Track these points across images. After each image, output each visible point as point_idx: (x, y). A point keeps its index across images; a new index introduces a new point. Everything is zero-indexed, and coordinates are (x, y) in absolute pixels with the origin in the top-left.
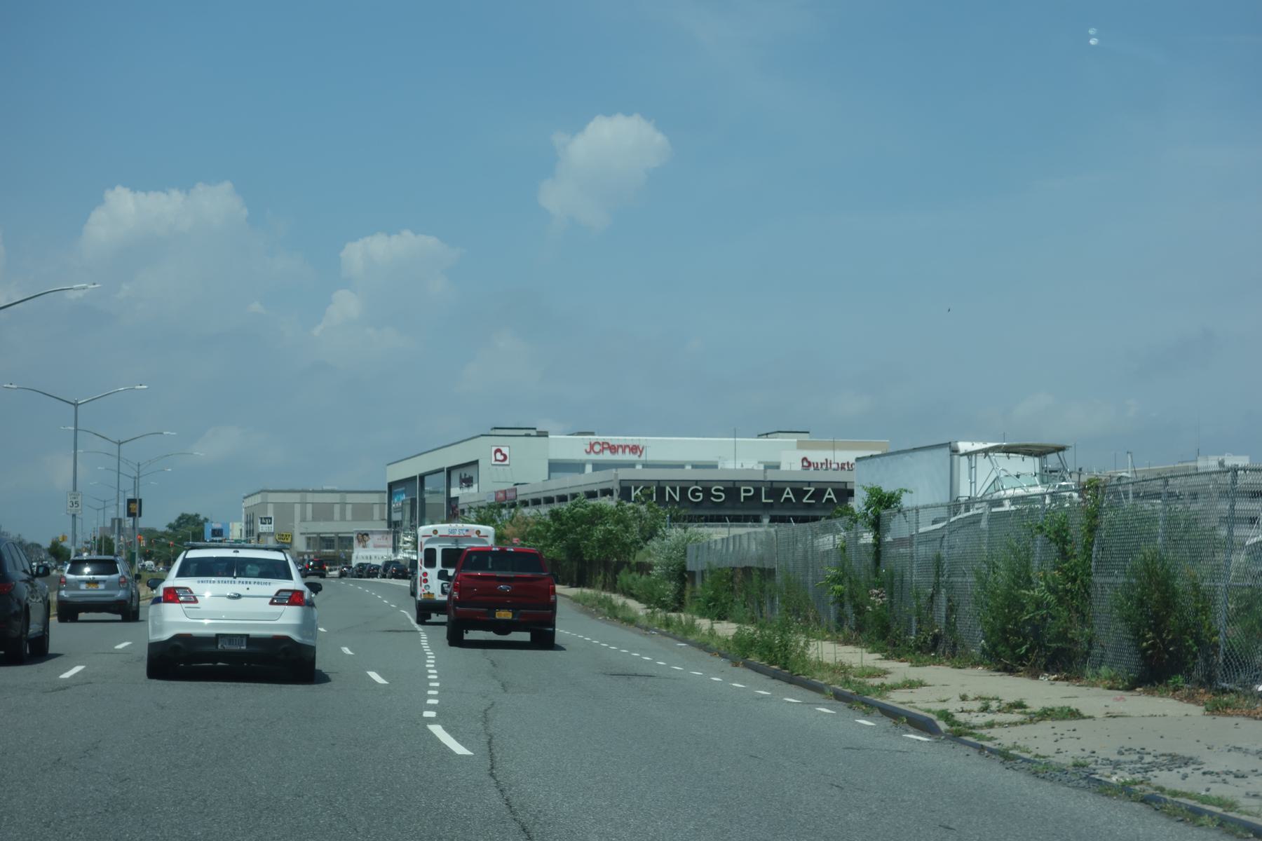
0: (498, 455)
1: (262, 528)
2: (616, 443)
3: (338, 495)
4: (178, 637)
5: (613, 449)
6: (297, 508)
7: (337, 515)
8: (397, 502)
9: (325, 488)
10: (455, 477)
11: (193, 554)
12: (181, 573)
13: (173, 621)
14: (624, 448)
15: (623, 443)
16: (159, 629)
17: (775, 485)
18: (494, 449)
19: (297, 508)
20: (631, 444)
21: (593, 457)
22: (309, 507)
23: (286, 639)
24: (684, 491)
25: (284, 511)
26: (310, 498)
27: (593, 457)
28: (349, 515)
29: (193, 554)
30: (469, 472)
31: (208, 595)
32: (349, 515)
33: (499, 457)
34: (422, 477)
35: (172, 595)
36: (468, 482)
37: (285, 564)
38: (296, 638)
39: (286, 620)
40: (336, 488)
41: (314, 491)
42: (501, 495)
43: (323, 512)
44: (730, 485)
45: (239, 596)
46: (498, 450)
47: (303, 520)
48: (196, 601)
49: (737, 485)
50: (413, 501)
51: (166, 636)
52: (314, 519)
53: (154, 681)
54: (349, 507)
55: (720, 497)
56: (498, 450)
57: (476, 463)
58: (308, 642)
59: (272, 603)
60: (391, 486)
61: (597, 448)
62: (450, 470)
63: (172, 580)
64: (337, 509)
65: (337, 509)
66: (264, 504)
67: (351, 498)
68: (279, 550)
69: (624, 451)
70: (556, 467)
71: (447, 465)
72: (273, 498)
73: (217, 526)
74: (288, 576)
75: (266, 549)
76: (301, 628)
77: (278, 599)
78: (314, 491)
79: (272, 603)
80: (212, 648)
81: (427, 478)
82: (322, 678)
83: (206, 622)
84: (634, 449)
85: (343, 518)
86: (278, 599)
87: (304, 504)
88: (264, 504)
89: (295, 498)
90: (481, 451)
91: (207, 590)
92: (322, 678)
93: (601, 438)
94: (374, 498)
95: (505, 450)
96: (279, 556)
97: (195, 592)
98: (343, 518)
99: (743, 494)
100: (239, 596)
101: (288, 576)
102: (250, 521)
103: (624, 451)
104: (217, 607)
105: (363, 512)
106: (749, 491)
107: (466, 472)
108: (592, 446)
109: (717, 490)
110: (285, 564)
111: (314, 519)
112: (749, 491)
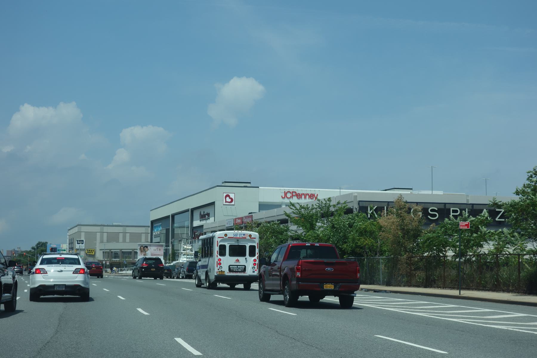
0: (228, 198)
1: (77, 246)
2: (301, 193)
3: (121, 228)
4: (41, 286)
5: (299, 196)
6: (98, 235)
7: (121, 239)
8: (156, 232)
9: (114, 224)
10: (197, 214)
11: (45, 257)
12: (41, 264)
13: (39, 280)
14: (305, 195)
15: (305, 193)
16: (34, 283)
17: (475, 207)
18: (225, 195)
19: (98, 235)
20: (310, 193)
21: (286, 201)
22: (105, 235)
23: (79, 286)
24: (425, 211)
25: (91, 236)
26: (106, 229)
27: (286, 201)
28: (128, 239)
29: (45, 257)
30: (206, 210)
31: (52, 271)
32: (128, 239)
33: (228, 200)
34: (173, 216)
35: (38, 271)
36: (203, 217)
37: (78, 259)
38: (82, 285)
39: (79, 279)
40: (121, 224)
41: (108, 226)
42: (239, 221)
43: (113, 237)
44: (442, 207)
45: (62, 271)
46: (228, 196)
47: (102, 242)
48: (47, 273)
49: (447, 206)
50: (167, 230)
51: (36, 285)
52: (108, 241)
53: (32, 302)
54: (128, 235)
55: (435, 216)
56: (228, 196)
57: (213, 204)
58: (86, 286)
59: (73, 273)
60: (153, 222)
61: (289, 195)
62: (193, 210)
63: (38, 266)
64: (121, 236)
65: (121, 236)
66: (80, 232)
67: (129, 230)
68: (76, 254)
69: (305, 198)
70: (263, 206)
71: (191, 207)
72: (84, 229)
73: (54, 246)
74: (79, 264)
75: (71, 254)
76: (85, 282)
77: (76, 272)
78: (108, 226)
79: (73, 273)
80: (52, 289)
81: (176, 216)
82: (91, 300)
83: (52, 280)
84: (312, 196)
85: (124, 241)
86: (76, 272)
87: (102, 233)
88: (80, 232)
89: (98, 229)
90: (217, 196)
91: (52, 269)
92: (91, 300)
93: (291, 189)
94: (142, 230)
95: (232, 196)
96: (76, 257)
97: (46, 270)
98: (124, 241)
99: (452, 214)
100: (62, 271)
101: (79, 264)
102: (71, 243)
103: (305, 198)
104: (54, 275)
105: (135, 237)
106: (457, 211)
107: (205, 210)
108: (286, 194)
109: (432, 210)
110: (78, 259)
111: (108, 241)
112: (457, 211)
